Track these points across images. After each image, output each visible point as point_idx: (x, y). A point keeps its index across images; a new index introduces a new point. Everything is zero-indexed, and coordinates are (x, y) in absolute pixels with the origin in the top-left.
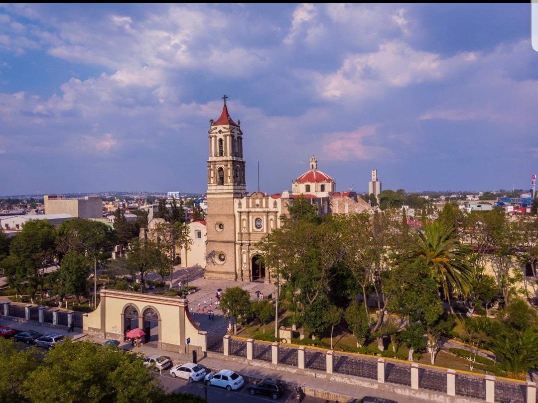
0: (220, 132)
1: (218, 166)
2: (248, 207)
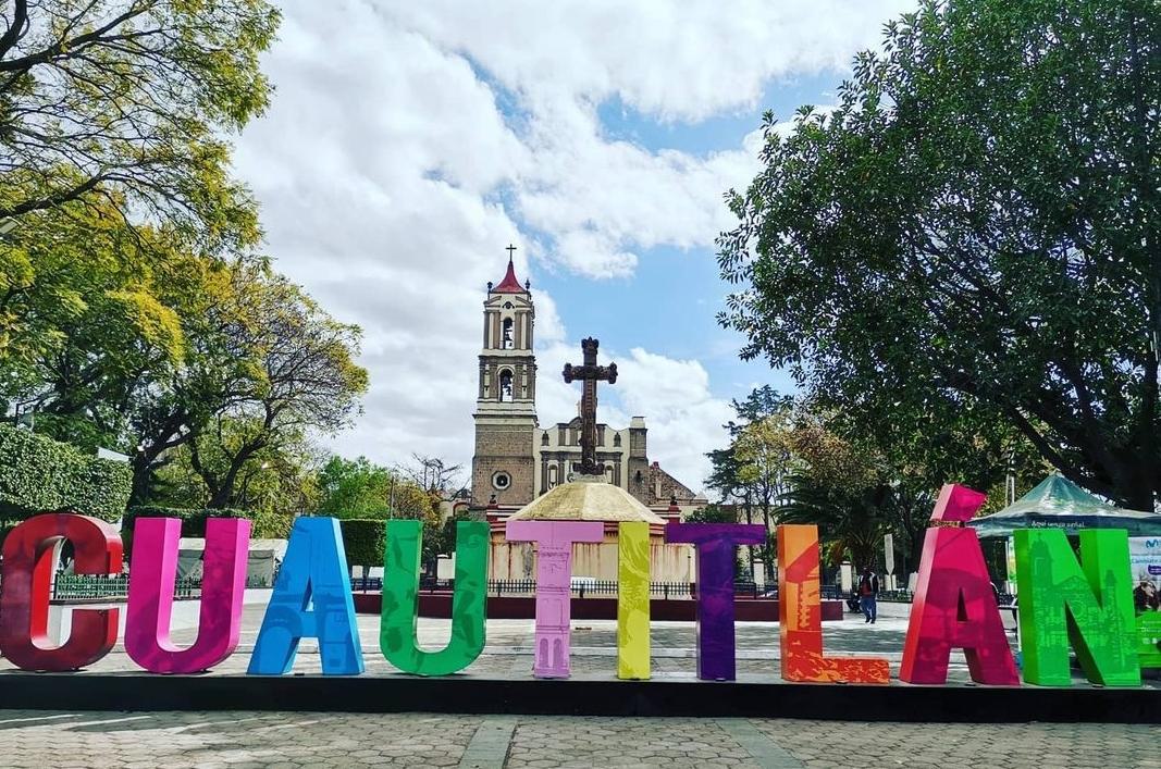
0: (508, 305)
1: (501, 367)
2: (562, 443)
